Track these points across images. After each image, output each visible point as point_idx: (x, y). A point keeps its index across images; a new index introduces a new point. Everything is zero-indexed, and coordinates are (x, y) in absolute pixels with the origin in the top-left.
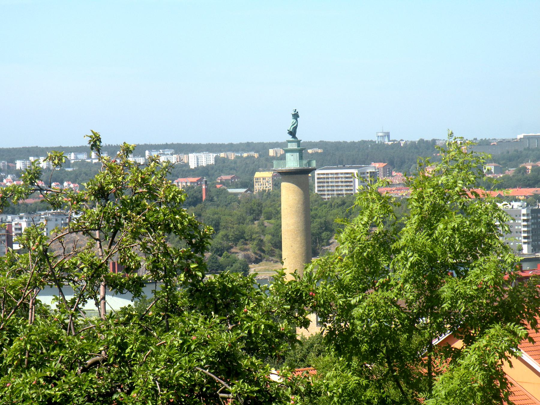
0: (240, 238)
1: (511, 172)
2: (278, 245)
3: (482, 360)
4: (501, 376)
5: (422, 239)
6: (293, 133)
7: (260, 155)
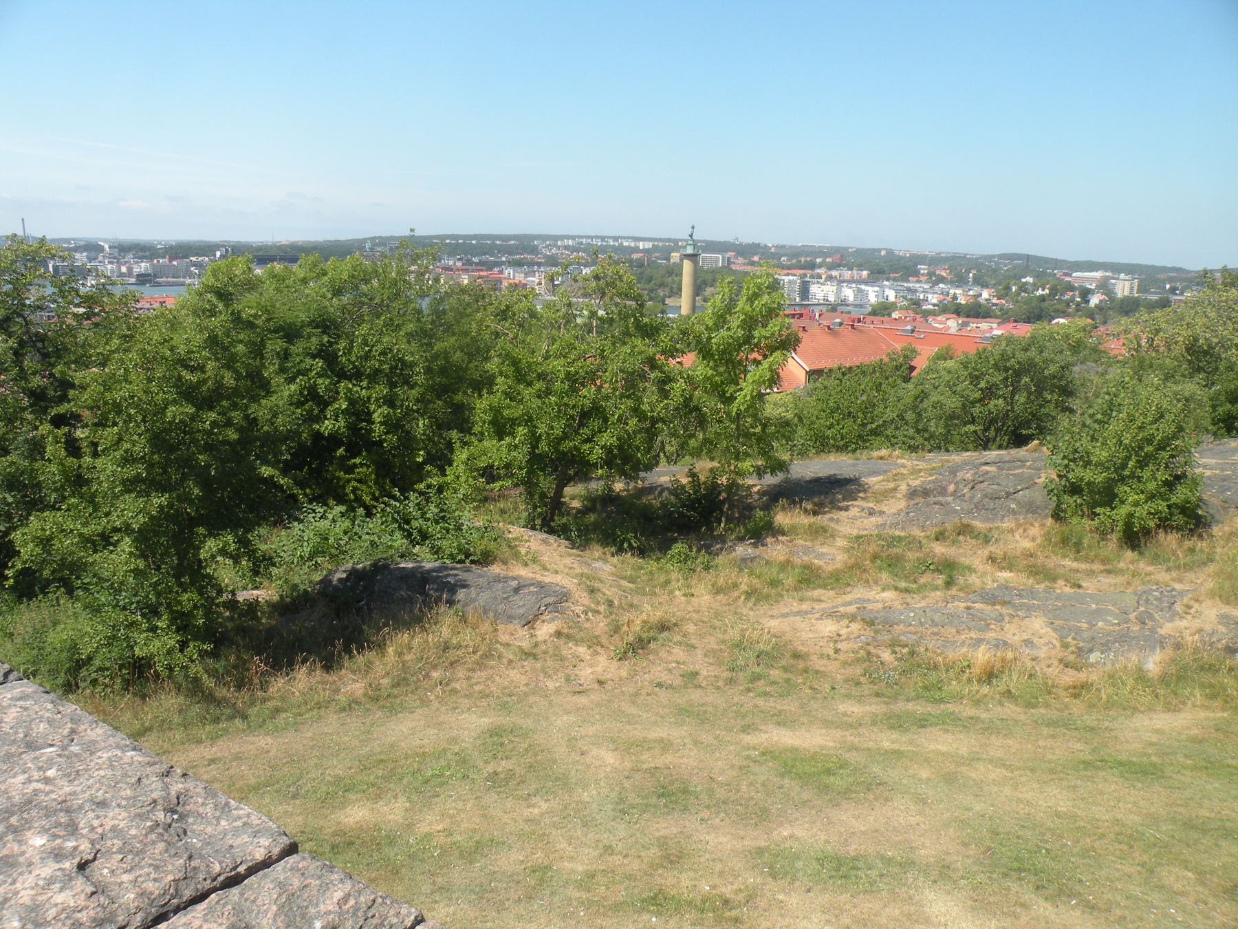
0: (662, 285)
1: (794, 261)
2: (680, 290)
3: (770, 367)
4: (778, 374)
5: (748, 308)
6: (691, 236)
7: (675, 245)
